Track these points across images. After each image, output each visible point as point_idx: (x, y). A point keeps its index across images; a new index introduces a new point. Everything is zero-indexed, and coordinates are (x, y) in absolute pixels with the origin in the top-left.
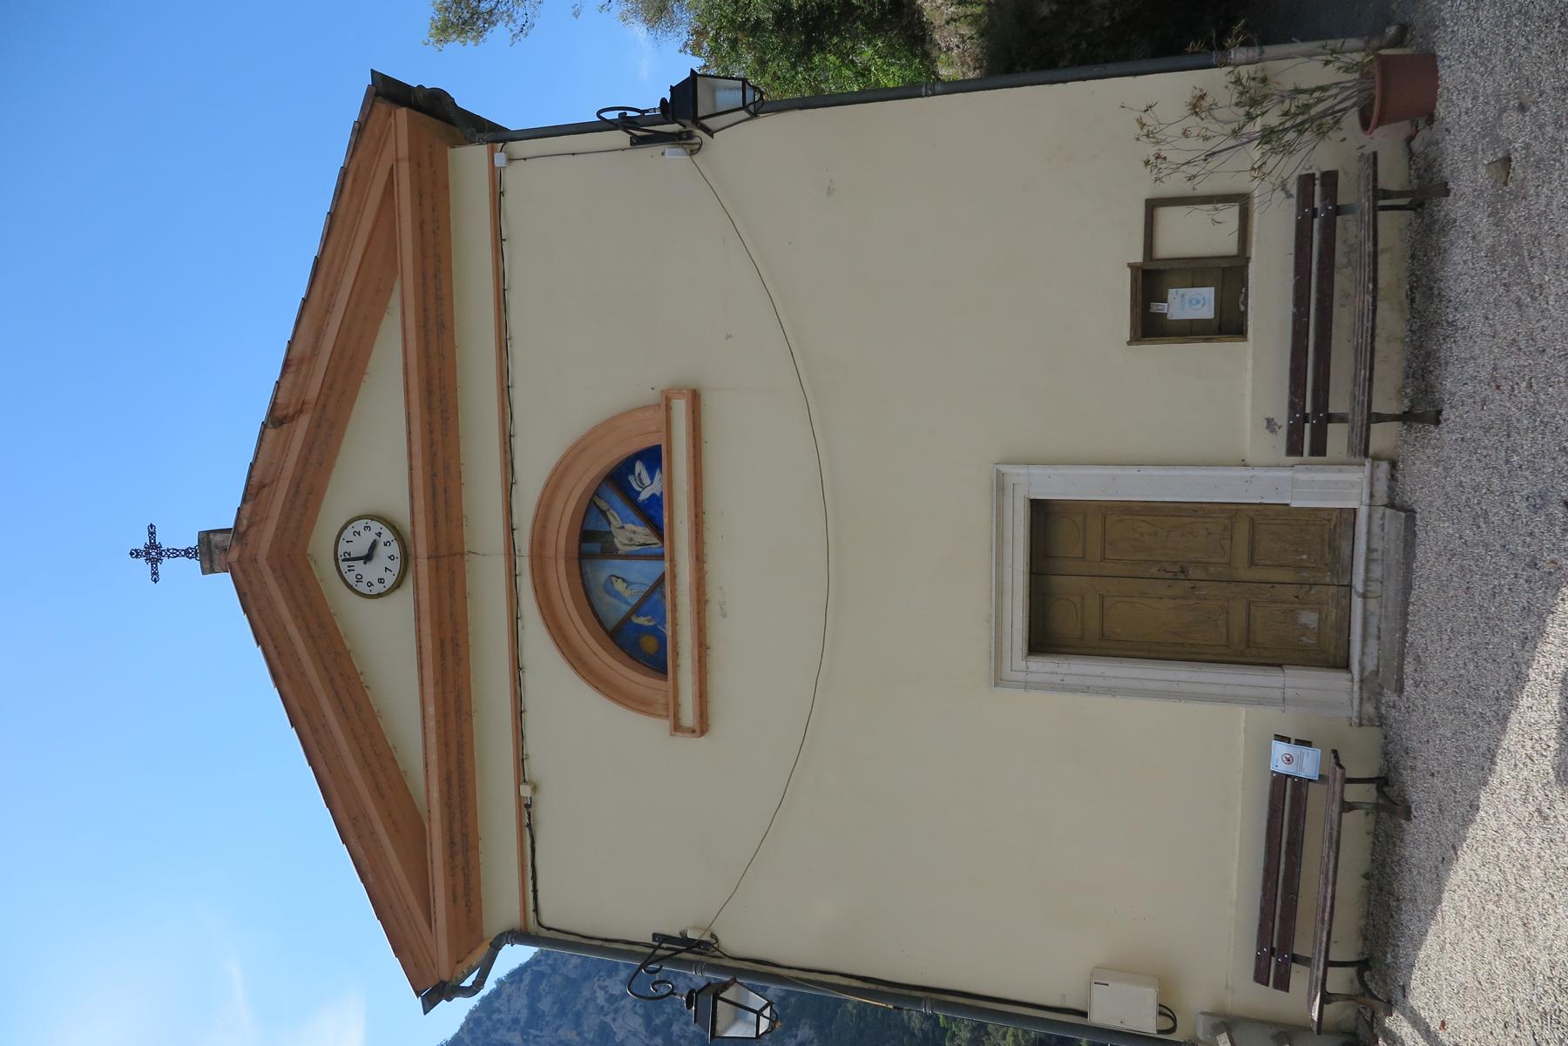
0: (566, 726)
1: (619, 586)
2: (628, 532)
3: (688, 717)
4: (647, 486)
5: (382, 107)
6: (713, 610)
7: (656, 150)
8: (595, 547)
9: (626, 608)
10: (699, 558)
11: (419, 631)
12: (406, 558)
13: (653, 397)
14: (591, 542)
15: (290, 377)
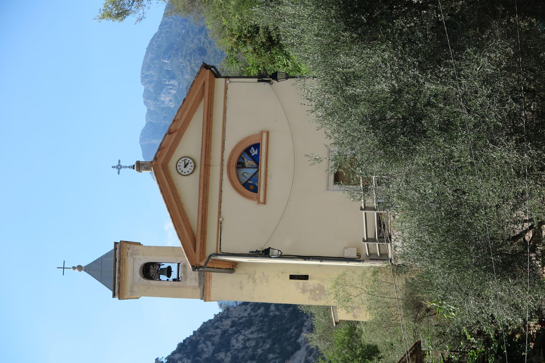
0: (233, 204)
1: (245, 174)
2: (249, 162)
3: (262, 200)
4: (254, 152)
5: (204, 69)
6: (268, 177)
7: (263, 83)
8: (240, 166)
9: (247, 179)
10: (266, 166)
11: (200, 181)
12: (195, 166)
13: (258, 132)
14: (240, 165)
15: (174, 124)
